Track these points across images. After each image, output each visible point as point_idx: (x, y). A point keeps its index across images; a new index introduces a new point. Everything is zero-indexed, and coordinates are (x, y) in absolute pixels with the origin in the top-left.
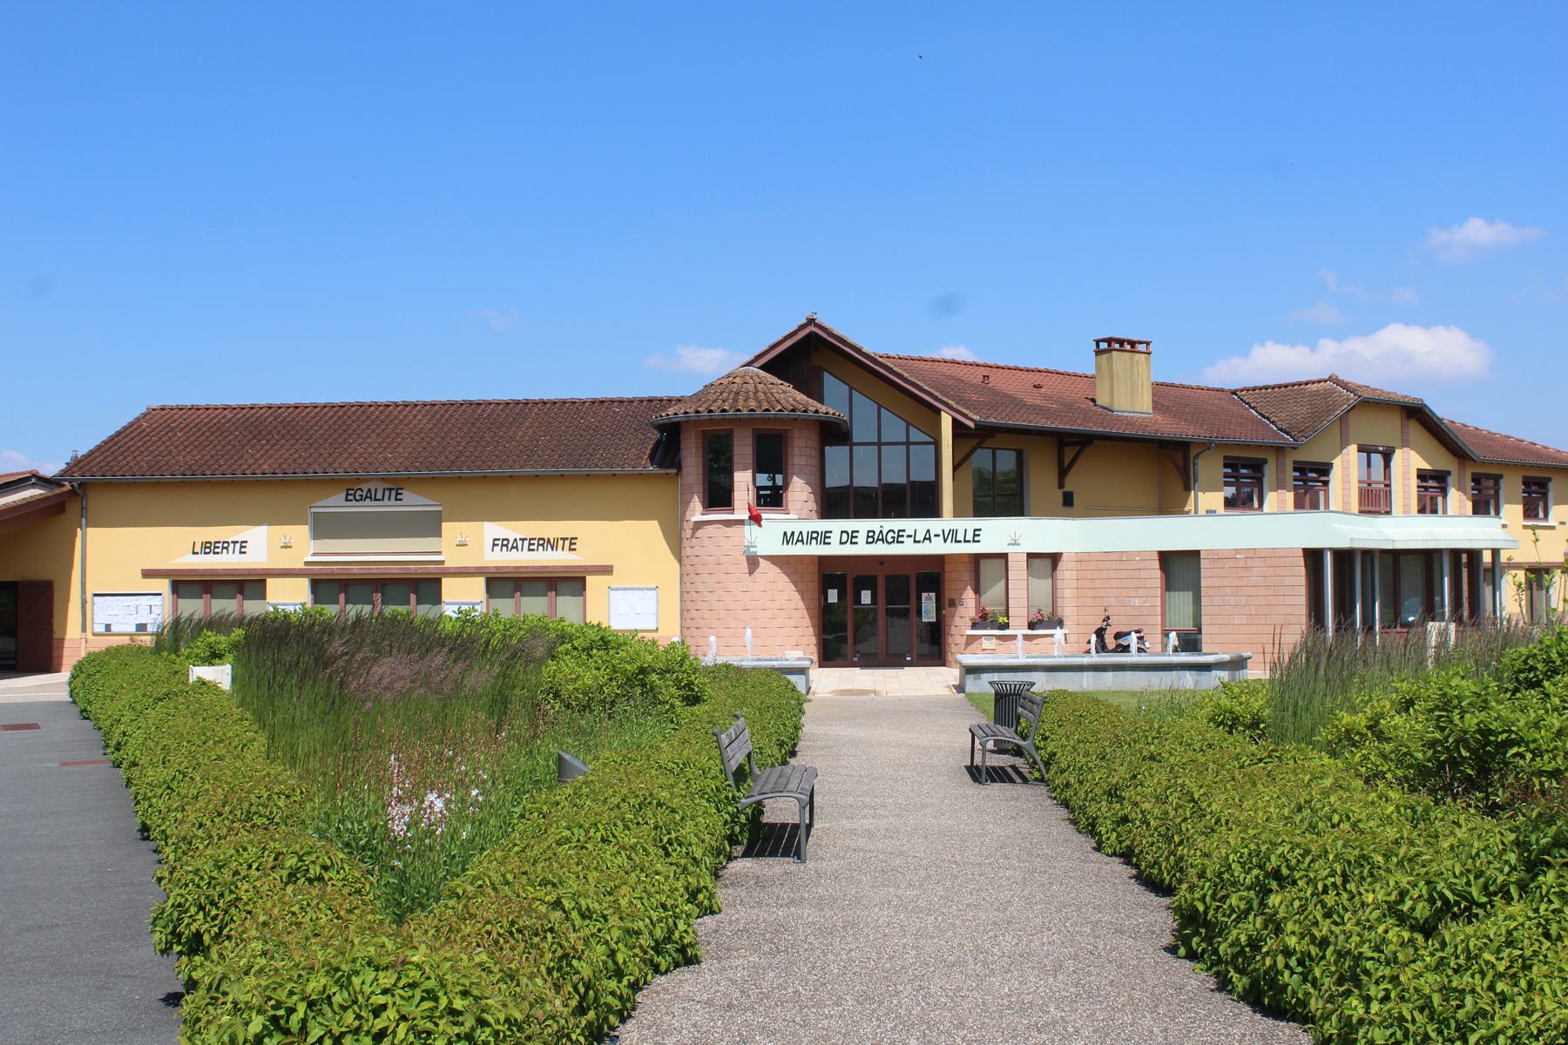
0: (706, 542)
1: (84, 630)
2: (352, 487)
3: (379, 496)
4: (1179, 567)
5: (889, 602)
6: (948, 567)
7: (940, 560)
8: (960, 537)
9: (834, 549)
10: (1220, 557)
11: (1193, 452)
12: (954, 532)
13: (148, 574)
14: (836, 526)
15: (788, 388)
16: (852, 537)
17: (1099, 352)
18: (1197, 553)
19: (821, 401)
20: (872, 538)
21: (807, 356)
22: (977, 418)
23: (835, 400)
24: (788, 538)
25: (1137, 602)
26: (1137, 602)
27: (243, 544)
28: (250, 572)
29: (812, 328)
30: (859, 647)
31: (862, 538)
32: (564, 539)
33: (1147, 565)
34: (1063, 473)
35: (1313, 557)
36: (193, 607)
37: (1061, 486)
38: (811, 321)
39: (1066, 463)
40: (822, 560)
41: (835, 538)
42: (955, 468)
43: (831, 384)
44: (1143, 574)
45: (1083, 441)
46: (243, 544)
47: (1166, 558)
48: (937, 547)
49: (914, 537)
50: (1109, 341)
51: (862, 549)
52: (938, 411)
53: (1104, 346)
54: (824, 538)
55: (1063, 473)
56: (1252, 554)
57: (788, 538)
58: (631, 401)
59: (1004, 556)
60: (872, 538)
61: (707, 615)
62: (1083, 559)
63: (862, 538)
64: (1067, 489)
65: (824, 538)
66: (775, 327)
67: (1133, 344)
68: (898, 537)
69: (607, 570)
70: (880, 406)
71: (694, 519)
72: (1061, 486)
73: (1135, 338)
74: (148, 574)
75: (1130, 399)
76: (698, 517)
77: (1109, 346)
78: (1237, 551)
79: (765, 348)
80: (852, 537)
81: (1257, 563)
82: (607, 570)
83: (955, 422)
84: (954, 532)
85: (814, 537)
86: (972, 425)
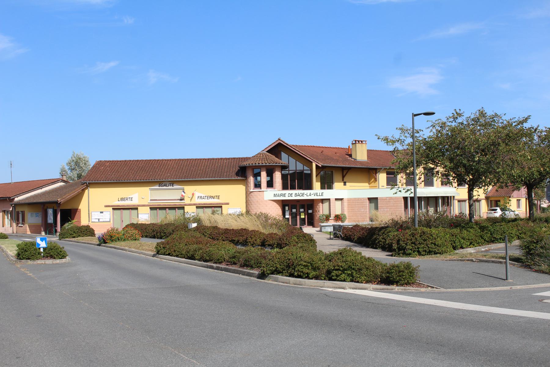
2: (160, 183)
4: (373, 200)
6: (315, 202)
7: (312, 201)
9: (287, 198)
10: (382, 199)
12: (317, 194)
13: (106, 206)
14: (287, 192)
15: (274, 157)
16: (291, 195)
17: (352, 144)
18: (377, 198)
19: (281, 159)
20: (296, 195)
21: (278, 149)
23: (285, 159)
24: (275, 195)
25: (363, 210)
26: (363, 210)
27: (132, 198)
29: (279, 141)
30: (66, 225)
31: (294, 195)
34: (343, 177)
35: (405, 199)
38: (279, 139)
40: (283, 201)
41: (287, 195)
42: (316, 176)
46: (132, 198)
47: (370, 200)
48: (312, 197)
50: (355, 141)
51: (294, 198)
52: (312, 162)
53: (354, 142)
55: (343, 177)
57: (275, 195)
58: (229, 159)
59: (329, 199)
60: (296, 195)
62: (349, 200)
63: (294, 195)
66: (270, 141)
67: (362, 142)
68: (303, 195)
69: (228, 204)
72: (343, 180)
74: (106, 206)
76: (252, 190)
77: (355, 142)
80: (291, 195)
81: (392, 200)
82: (228, 204)
83: (316, 165)
84: (317, 194)
85: (281, 195)
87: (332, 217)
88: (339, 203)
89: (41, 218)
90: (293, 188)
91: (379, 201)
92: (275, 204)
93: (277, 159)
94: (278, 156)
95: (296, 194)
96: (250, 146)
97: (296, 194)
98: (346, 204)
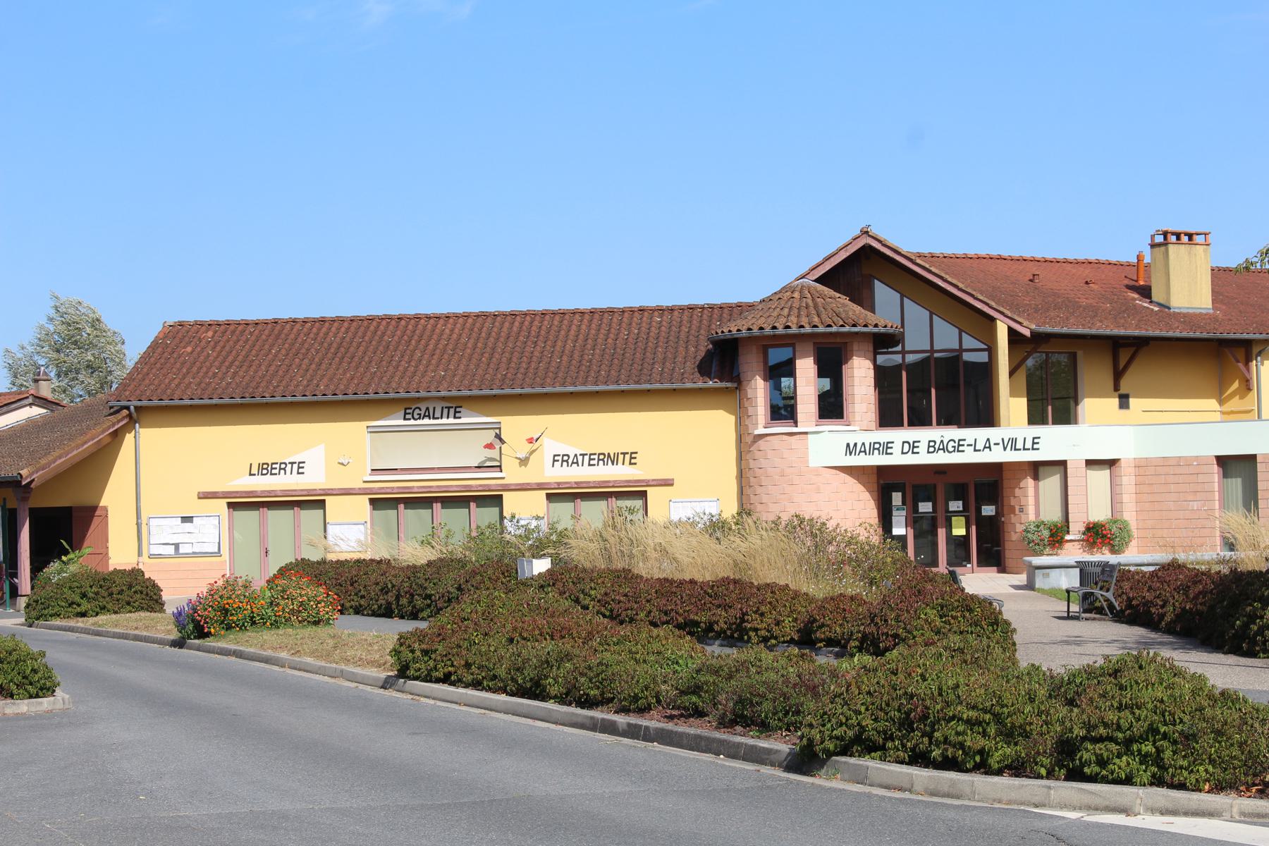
0: (770, 454)
1: (140, 554)
3: (438, 414)
6: (1006, 475)
7: (998, 467)
8: (1020, 445)
11: (1255, 350)
15: (844, 300)
16: (913, 447)
17: (1153, 246)
18: (1252, 458)
19: (873, 311)
21: (861, 268)
22: (1033, 327)
24: (850, 449)
25: (1195, 505)
26: (1195, 505)
27: (300, 465)
28: (310, 492)
31: (923, 447)
32: (624, 454)
33: (1205, 469)
34: (1118, 376)
37: (1116, 388)
38: (865, 233)
40: (881, 470)
41: (896, 449)
42: (1011, 373)
43: (884, 294)
45: (1139, 345)
46: (300, 465)
47: (1226, 463)
48: (997, 456)
49: (969, 446)
51: (923, 458)
52: (993, 320)
53: (1159, 239)
55: (1118, 376)
57: (850, 449)
58: (671, 310)
60: (932, 447)
62: (1142, 465)
63: (923, 447)
64: (1122, 391)
65: (886, 448)
66: (830, 241)
67: (1190, 236)
69: (668, 483)
70: (961, 331)
71: (756, 432)
72: (1116, 388)
75: (1188, 291)
76: (760, 430)
79: (820, 259)
80: (913, 447)
82: (668, 483)
85: (874, 448)
86: (1027, 333)
90: (919, 420)
93: (858, 309)
94: (863, 297)
96: (757, 262)
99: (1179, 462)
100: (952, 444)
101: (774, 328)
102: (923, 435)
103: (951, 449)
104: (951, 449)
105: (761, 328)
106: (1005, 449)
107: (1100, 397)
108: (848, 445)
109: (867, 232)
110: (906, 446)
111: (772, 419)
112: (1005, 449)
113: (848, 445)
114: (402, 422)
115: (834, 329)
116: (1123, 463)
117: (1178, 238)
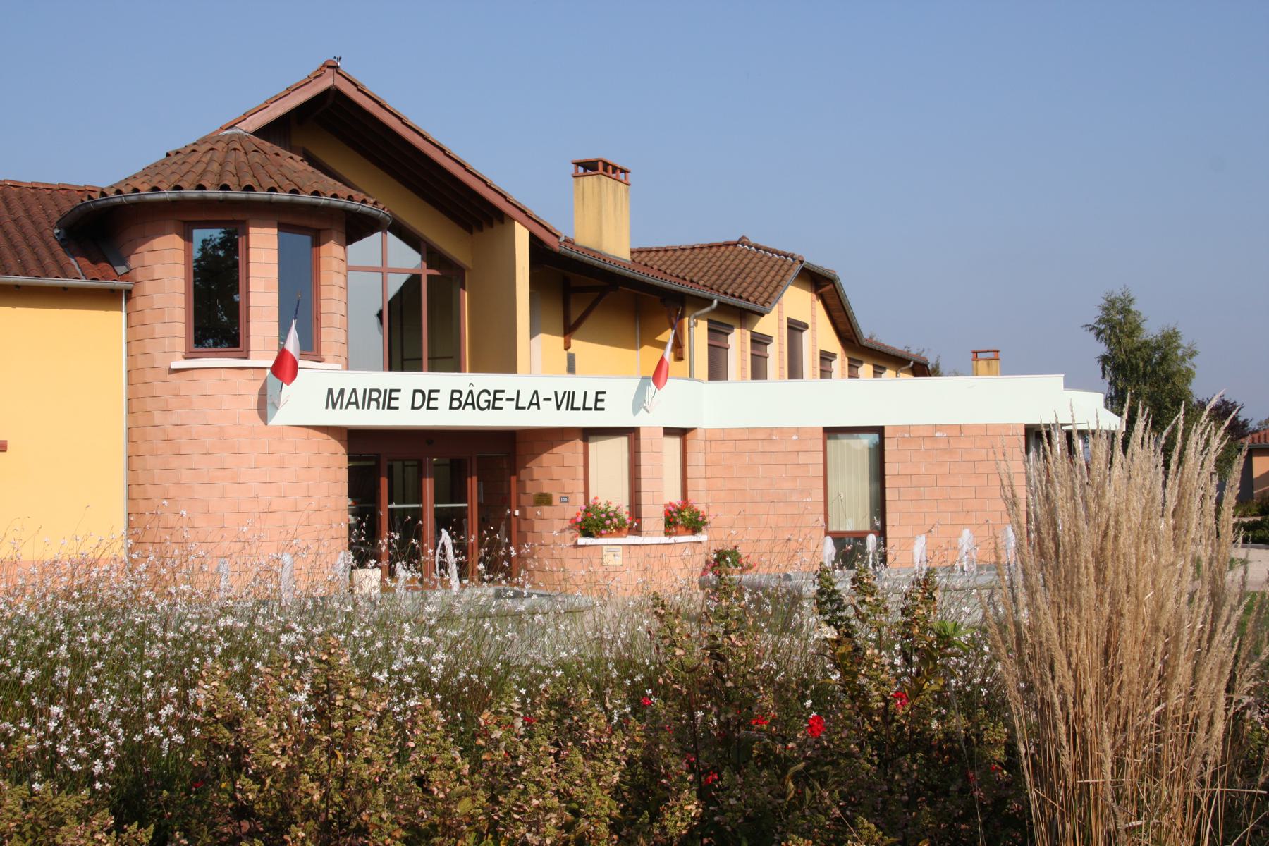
5: (436, 501)
8: (578, 403)
9: (404, 417)
10: (911, 434)
12: (570, 396)
13: (397, 408)
14: (407, 381)
16: (429, 398)
20: (458, 401)
24: (334, 399)
31: (443, 400)
36: (398, 524)
39: (573, 319)
41: (404, 400)
44: (803, 458)
48: (506, 418)
54: (389, 399)
56: (958, 431)
57: (334, 399)
60: (458, 401)
61: (200, 522)
62: (721, 437)
63: (443, 400)
65: (389, 399)
67: (615, 169)
73: (619, 165)
74: (397, 408)
78: (937, 428)
80: (429, 398)
85: (370, 398)
87: (653, 515)
88: (675, 442)
89: (618, 262)
90: (447, 361)
91: (642, 436)
92: (323, 436)
95: (455, 395)
97: (455, 395)
98: (694, 443)
99: (770, 435)
100: (484, 396)
101: (201, 187)
102: (444, 382)
103: (484, 405)
104: (484, 405)
105: (136, 190)
106: (559, 407)
107: (593, 341)
108: (330, 391)
109: (336, 67)
110: (419, 396)
111: (238, 346)
112: (559, 407)
113: (330, 391)
114: (665, 540)
115: (323, 200)
116: (700, 435)
117: (605, 170)
